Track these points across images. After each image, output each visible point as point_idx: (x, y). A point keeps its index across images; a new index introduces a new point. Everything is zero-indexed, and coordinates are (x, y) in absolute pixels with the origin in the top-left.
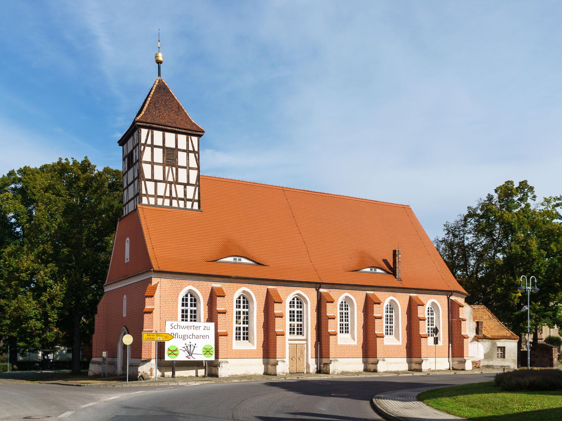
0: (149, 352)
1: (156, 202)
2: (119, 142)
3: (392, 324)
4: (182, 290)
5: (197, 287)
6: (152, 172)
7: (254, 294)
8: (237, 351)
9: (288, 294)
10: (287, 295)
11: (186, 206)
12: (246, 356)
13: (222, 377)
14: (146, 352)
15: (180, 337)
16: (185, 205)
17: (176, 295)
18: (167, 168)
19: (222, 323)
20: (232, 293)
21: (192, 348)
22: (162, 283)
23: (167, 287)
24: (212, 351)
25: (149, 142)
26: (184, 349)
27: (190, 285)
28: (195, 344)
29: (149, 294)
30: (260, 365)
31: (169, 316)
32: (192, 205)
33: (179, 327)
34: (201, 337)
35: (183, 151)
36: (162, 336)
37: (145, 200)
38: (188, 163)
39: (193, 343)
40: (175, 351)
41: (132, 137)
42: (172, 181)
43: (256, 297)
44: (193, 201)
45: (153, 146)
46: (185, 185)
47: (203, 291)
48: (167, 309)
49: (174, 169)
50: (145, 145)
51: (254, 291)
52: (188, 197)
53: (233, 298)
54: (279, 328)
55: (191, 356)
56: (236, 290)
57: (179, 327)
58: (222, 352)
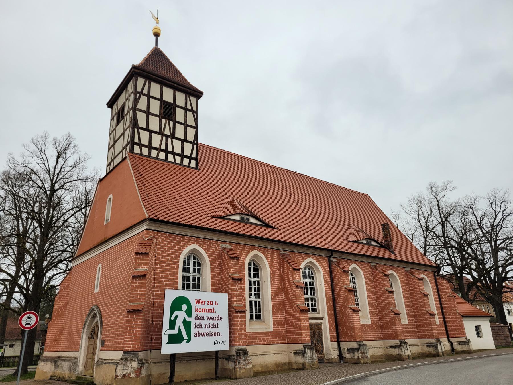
0: (375, 279)
1: (150, 153)
2: (107, 104)
3: (183, 277)
4: (185, 248)
7: (267, 259)
8: (252, 334)
12: (261, 341)
14: (130, 341)
16: (182, 161)
18: (164, 121)
25: (145, 91)
27: (194, 243)
29: (142, 251)
31: (166, 284)
35: (181, 108)
41: (125, 90)
42: (169, 134)
43: (269, 264)
44: (190, 158)
45: (149, 97)
46: (183, 141)
48: (163, 273)
49: (171, 123)
52: (185, 153)
56: (247, 253)
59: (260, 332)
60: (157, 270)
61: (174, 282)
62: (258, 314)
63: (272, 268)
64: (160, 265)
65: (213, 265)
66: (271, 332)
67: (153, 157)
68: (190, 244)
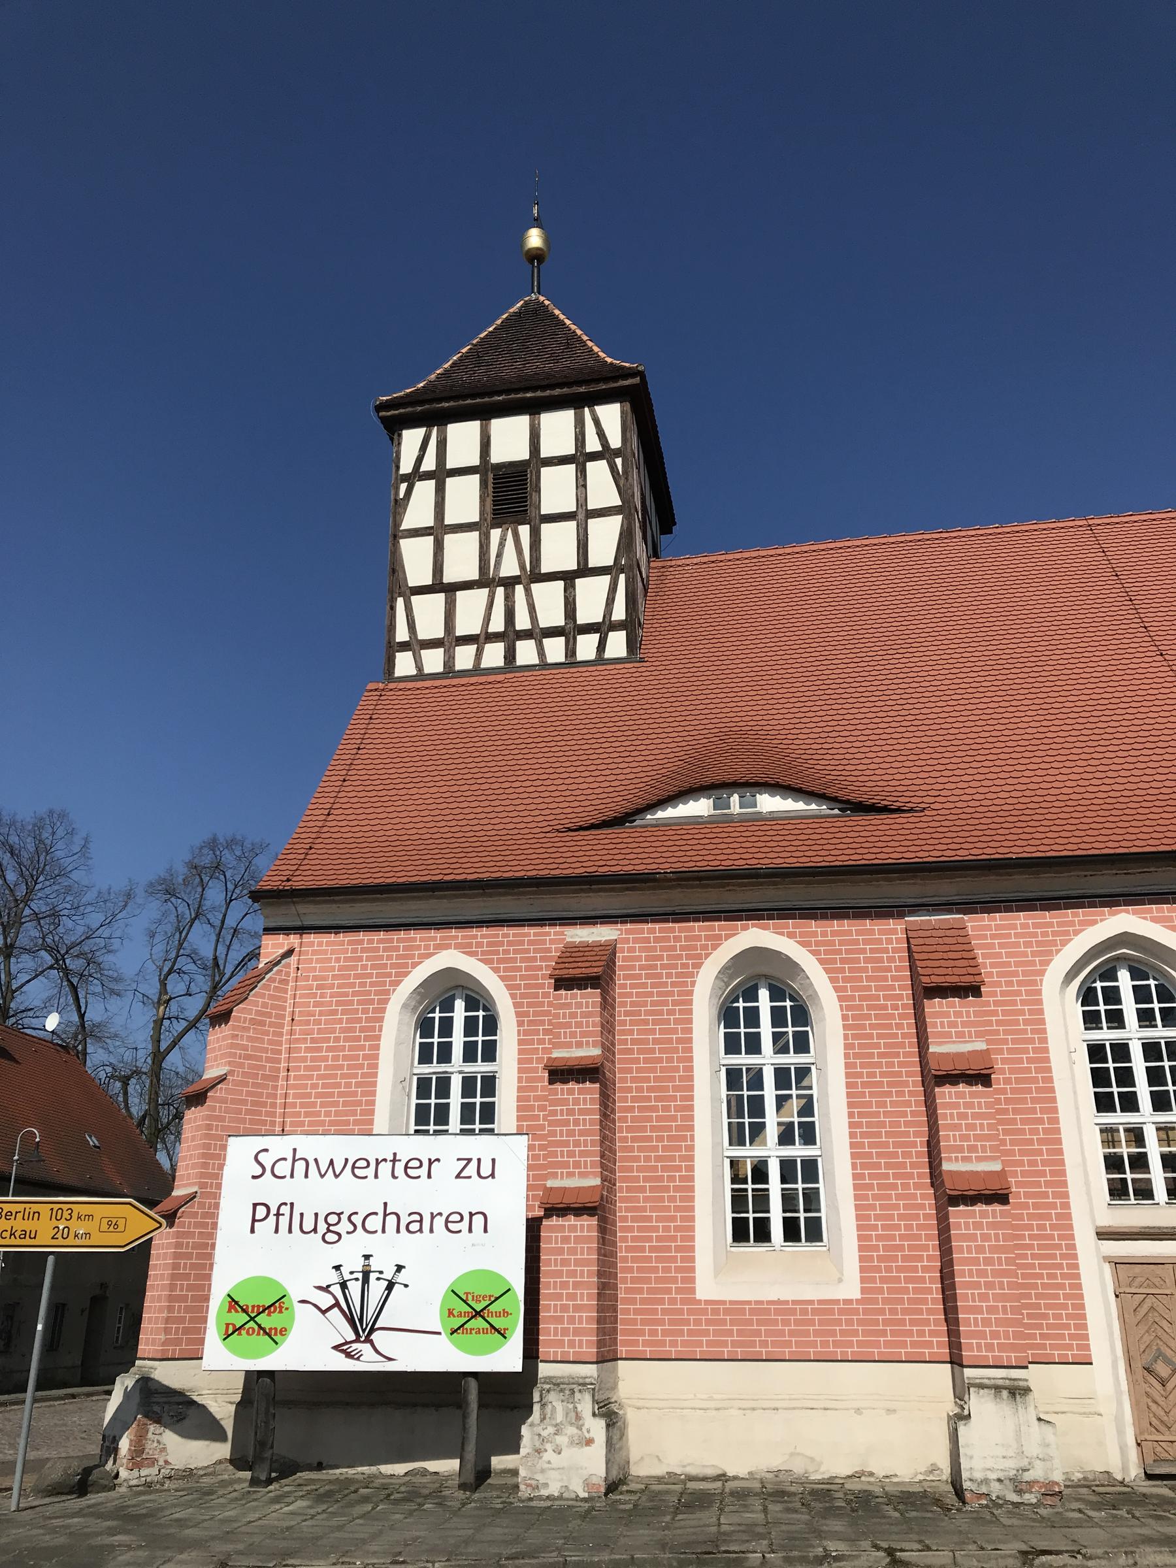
1: (571, 651)
5: (483, 953)
6: (528, 604)
8: (727, 1311)
9: (1054, 943)
10: (1047, 954)
11: (574, 653)
13: (544, 1492)
15: (308, 1225)
17: (372, 1002)
18: (496, 534)
19: (571, 1133)
20: (685, 966)
21: (377, 1289)
22: (307, 953)
23: (333, 969)
24: (505, 1313)
26: (325, 1301)
27: (448, 947)
28: (399, 1268)
30: (890, 1411)
31: (328, 1114)
32: (602, 646)
33: (300, 1166)
34: (439, 1222)
36: (90, 1216)
37: (404, 664)
38: (582, 500)
39: (383, 1264)
40: (267, 1309)
43: (832, 980)
44: (602, 628)
47: (519, 969)
49: (524, 531)
50: (418, 475)
51: (500, 961)
52: (582, 618)
53: (691, 993)
54: (972, 1149)
55: (368, 1340)
56: (704, 947)
57: (300, 1166)
58: (559, 1320)
59: (779, 1302)
60: (298, 1068)
61: (359, 1103)
62: (802, 1215)
63: (844, 989)
64: (308, 1050)
65: (530, 1023)
66: (848, 1302)
67: (458, 671)
68: (433, 954)
